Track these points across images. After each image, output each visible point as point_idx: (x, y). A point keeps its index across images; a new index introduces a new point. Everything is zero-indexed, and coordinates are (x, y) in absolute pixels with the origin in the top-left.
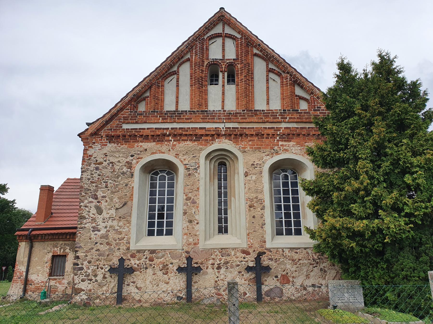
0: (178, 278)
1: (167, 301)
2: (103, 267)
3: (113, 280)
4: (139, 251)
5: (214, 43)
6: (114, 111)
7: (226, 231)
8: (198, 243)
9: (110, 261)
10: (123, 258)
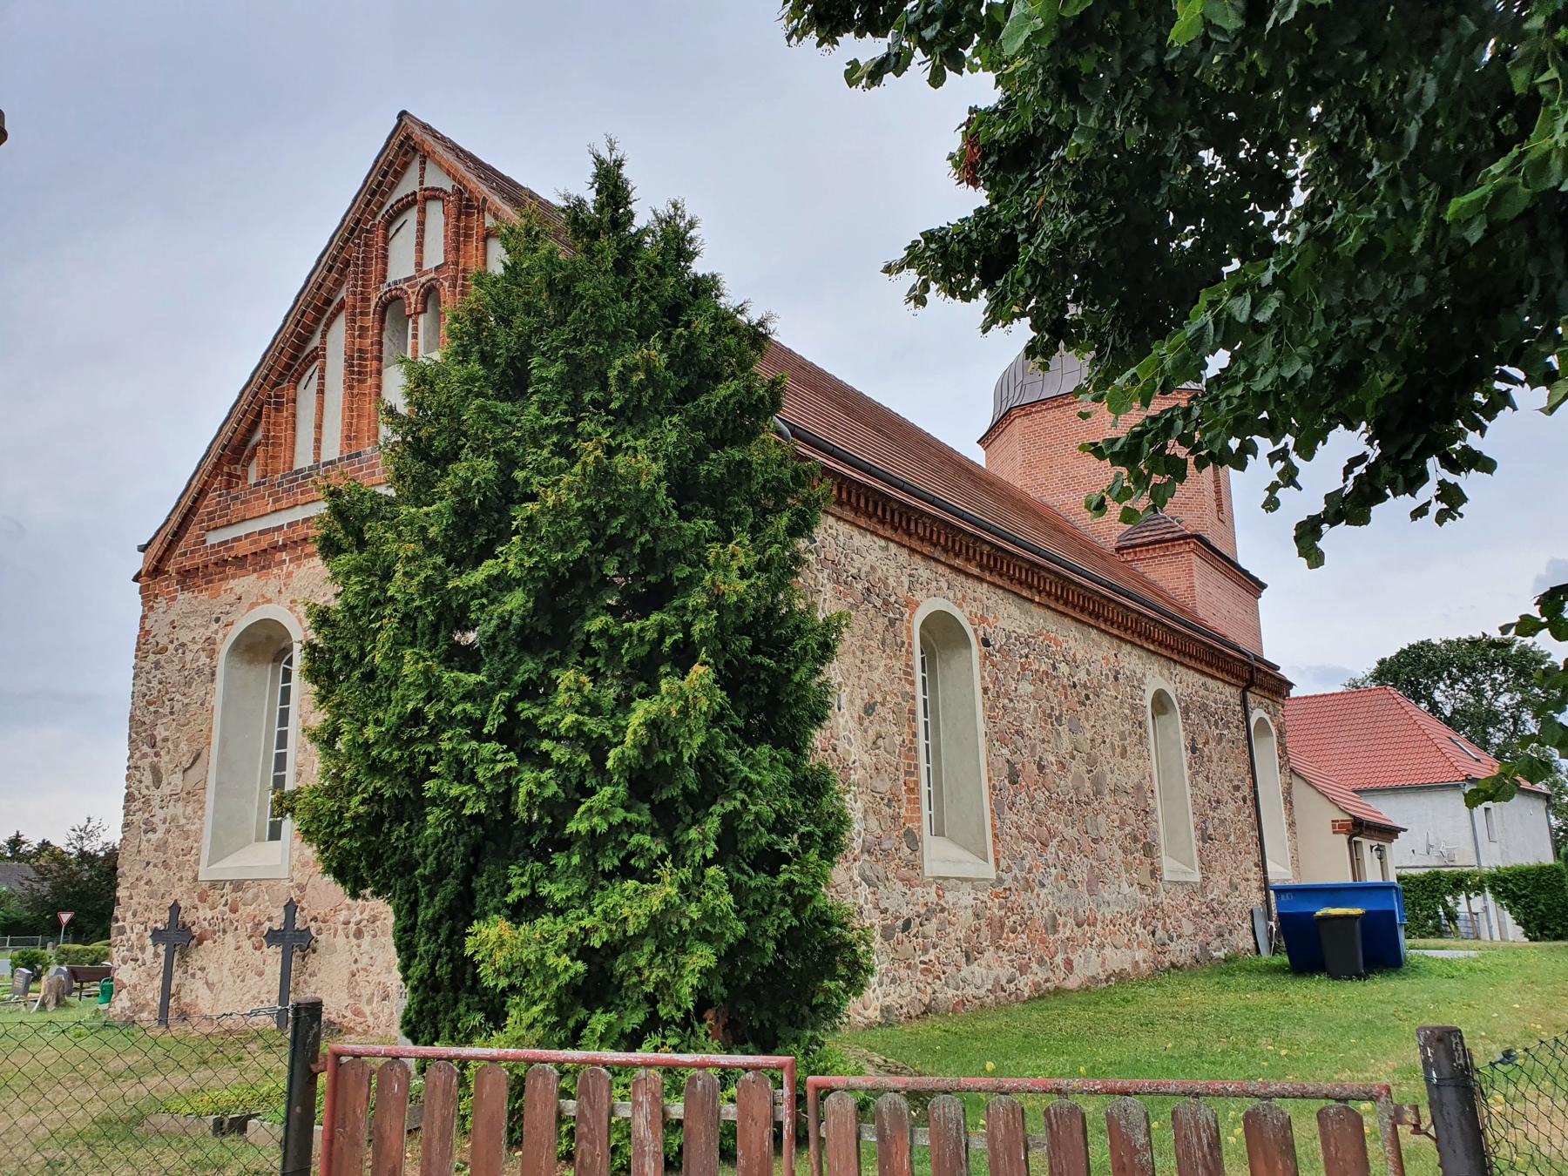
4: (214, 884)
5: (402, 231)
6: (187, 502)
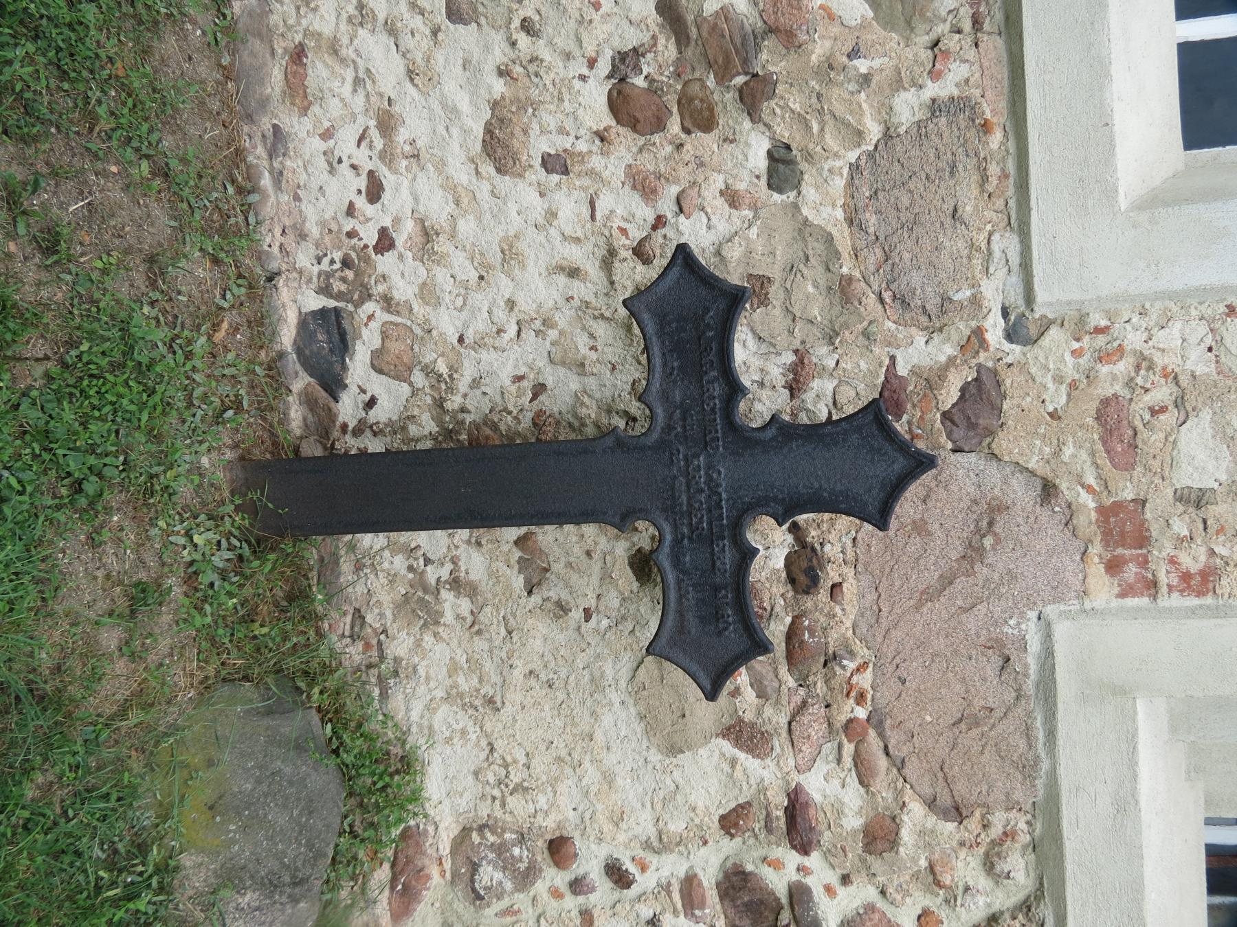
0: (581, 290)
1: (278, 177)
7: (1206, 824)
8: (1152, 586)
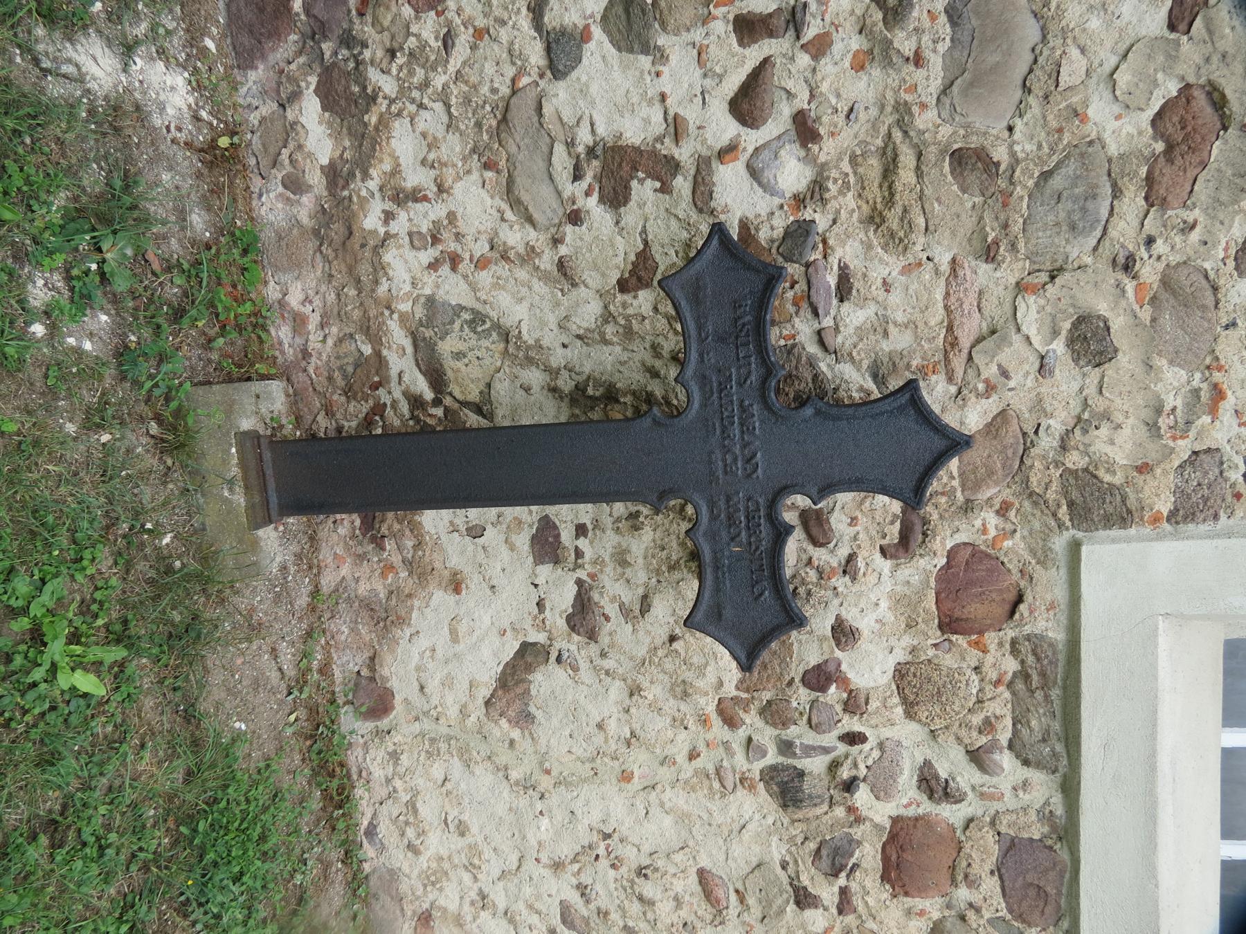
2: (778, 124)
3: (588, 312)
9: (875, 219)
10: (939, 460)
